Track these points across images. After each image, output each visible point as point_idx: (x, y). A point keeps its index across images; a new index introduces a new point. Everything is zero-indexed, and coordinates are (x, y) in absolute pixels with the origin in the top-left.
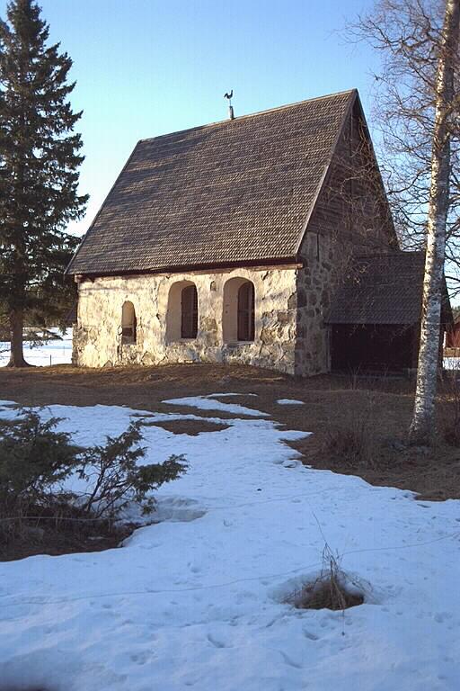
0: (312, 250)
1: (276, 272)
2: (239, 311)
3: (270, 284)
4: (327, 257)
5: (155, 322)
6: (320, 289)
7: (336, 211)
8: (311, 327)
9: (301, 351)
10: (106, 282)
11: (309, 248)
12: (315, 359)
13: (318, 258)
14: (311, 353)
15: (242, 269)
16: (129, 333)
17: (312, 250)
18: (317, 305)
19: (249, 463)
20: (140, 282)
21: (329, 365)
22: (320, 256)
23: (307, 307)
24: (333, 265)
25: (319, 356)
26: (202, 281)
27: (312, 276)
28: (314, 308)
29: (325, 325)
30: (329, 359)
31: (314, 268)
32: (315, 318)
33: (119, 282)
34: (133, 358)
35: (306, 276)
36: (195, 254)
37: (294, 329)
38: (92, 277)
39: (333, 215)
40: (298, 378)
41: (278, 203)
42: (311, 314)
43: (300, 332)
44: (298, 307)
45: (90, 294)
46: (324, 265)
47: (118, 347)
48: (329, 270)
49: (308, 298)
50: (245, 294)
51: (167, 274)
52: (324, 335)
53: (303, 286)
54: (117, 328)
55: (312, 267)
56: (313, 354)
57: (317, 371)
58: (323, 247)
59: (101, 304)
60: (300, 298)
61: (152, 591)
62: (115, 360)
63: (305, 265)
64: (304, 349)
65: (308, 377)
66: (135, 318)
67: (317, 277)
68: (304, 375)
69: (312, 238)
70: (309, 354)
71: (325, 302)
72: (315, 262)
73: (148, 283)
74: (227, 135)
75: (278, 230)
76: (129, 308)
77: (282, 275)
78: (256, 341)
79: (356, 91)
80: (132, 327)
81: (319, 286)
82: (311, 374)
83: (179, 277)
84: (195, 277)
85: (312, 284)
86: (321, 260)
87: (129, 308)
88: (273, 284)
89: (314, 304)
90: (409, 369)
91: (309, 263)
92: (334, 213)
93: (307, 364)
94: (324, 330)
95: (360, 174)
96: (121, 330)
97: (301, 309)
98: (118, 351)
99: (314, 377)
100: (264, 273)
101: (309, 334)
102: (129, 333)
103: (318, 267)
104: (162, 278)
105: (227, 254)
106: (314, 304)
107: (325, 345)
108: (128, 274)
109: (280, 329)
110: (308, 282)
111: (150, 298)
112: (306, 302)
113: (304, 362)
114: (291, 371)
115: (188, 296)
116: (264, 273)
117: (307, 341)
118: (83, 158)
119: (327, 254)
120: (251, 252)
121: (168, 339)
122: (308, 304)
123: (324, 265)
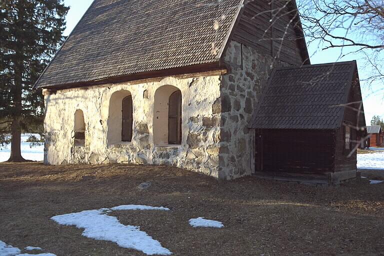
0: (236, 58)
1: (201, 79)
2: (169, 117)
3: (196, 90)
5: (99, 126)
6: (244, 96)
7: (258, 27)
8: (235, 132)
9: (225, 155)
10: (70, 93)
11: (233, 56)
12: (239, 161)
13: (241, 67)
15: (171, 78)
16: (80, 137)
17: (236, 58)
18: (241, 111)
19: (18, 226)
21: (253, 167)
22: (244, 65)
24: (256, 75)
25: (243, 159)
26: (136, 90)
28: (238, 113)
30: (253, 161)
31: (238, 76)
33: (80, 92)
34: (83, 158)
35: (230, 83)
36: (127, 66)
37: (218, 133)
38: (53, 90)
39: (255, 30)
40: (222, 182)
41: (205, 17)
42: (235, 119)
43: (225, 136)
44: (222, 112)
45: (57, 103)
46: (248, 74)
47: (72, 148)
48: (252, 79)
50: (173, 101)
51: (108, 85)
52: (247, 140)
53: (228, 91)
54: (71, 134)
55: (236, 74)
56: (238, 157)
57: (241, 173)
58: (247, 58)
59: (60, 110)
60: (224, 103)
62: (69, 160)
63: (229, 71)
65: (233, 181)
66: (85, 124)
67: (241, 85)
68: (229, 178)
69: (236, 47)
71: (248, 109)
72: (239, 71)
73: (91, 92)
75: (204, 39)
76: (79, 114)
77: (207, 82)
78: (183, 144)
81: (243, 93)
82: (235, 177)
83: (117, 88)
84: (131, 86)
86: (245, 69)
87: (79, 114)
88: (199, 91)
89: (238, 110)
90: (332, 174)
91: (233, 71)
92: (256, 28)
94: (247, 135)
95: (362, 112)
96: (73, 134)
97: (226, 114)
98: (72, 152)
99: (238, 180)
100: (190, 80)
101: (233, 138)
102: (80, 137)
103: (242, 75)
104: (103, 89)
105: (157, 64)
106: (238, 110)
107: (249, 150)
108: (85, 85)
109: (205, 134)
110: (232, 88)
111: (95, 105)
113: (228, 165)
114: (215, 174)
115: (126, 104)
116: (190, 80)
117: (231, 145)
118: (69, 8)
119: (250, 64)
120: (178, 60)
121: (110, 142)
123: (248, 74)
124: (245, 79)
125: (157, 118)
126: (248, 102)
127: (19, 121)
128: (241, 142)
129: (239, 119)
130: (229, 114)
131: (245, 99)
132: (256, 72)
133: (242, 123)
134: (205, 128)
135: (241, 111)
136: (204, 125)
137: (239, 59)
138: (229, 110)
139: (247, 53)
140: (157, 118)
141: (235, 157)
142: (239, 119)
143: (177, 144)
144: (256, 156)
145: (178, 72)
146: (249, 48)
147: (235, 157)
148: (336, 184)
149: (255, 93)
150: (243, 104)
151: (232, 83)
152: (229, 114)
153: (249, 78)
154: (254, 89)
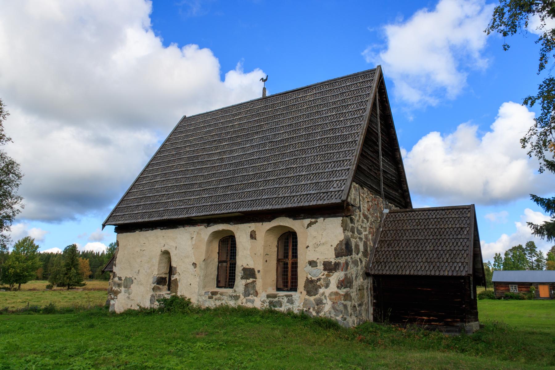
0: (355, 199)
4: (366, 209)
8: (356, 277)
14: (356, 304)
20: (226, 303)
22: (361, 206)
23: (353, 256)
26: (241, 232)
27: (356, 225)
29: (367, 275)
32: (359, 268)
35: (351, 225)
49: (353, 248)
53: (350, 234)
58: (363, 199)
61: (30, 290)
64: (351, 300)
70: (355, 306)
71: (365, 254)
74: (429, 316)
79: (474, 205)
80: (167, 276)
85: (356, 233)
86: (362, 211)
93: (354, 317)
106: (358, 254)
107: (368, 299)
112: (352, 251)
122: (354, 253)
124: (363, 222)
125: (266, 261)
126: (365, 245)
127: (369, 257)
128: (361, 289)
129: (359, 263)
130: (351, 258)
131: (363, 242)
132: (370, 214)
133: (362, 268)
134: (326, 273)
135: (360, 255)
136: (325, 270)
137: (358, 200)
138: (351, 254)
139: (363, 193)
140: (266, 261)
141: (357, 306)
142: (359, 263)
143: (291, 290)
144: (375, 305)
145: (296, 213)
146: (365, 189)
147: (357, 306)
148: (535, 151)
149: (370, 237)
150: (362, 248)
151: (353, 225)
152: (351, 258)
153: (365, 220)
154: (370, 233)
